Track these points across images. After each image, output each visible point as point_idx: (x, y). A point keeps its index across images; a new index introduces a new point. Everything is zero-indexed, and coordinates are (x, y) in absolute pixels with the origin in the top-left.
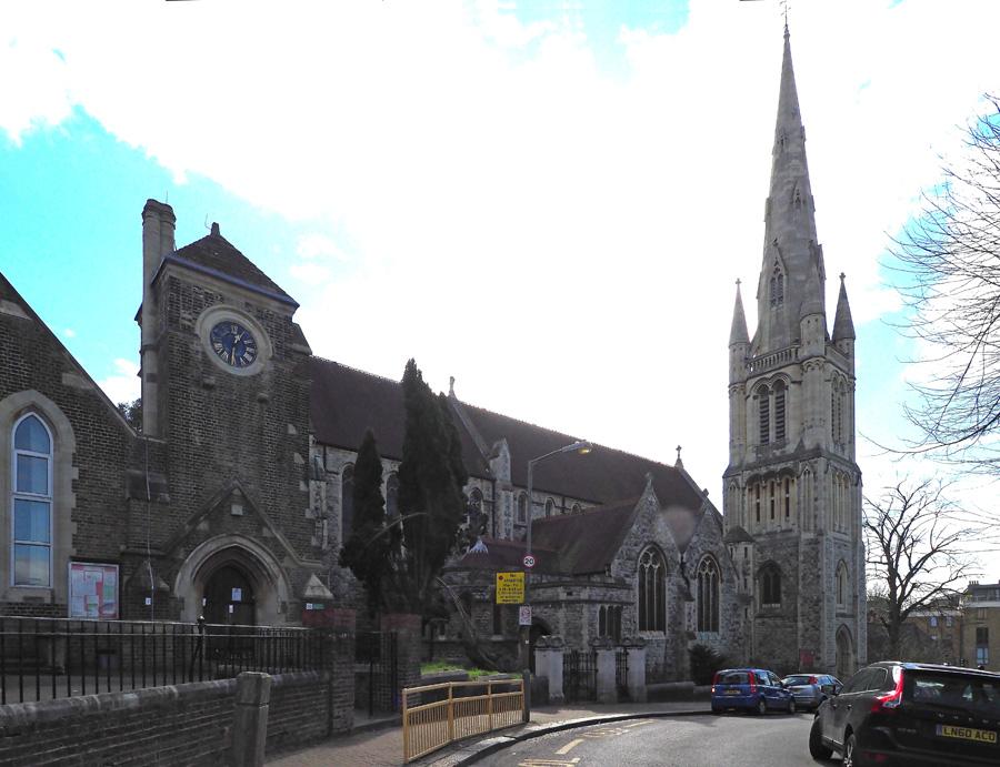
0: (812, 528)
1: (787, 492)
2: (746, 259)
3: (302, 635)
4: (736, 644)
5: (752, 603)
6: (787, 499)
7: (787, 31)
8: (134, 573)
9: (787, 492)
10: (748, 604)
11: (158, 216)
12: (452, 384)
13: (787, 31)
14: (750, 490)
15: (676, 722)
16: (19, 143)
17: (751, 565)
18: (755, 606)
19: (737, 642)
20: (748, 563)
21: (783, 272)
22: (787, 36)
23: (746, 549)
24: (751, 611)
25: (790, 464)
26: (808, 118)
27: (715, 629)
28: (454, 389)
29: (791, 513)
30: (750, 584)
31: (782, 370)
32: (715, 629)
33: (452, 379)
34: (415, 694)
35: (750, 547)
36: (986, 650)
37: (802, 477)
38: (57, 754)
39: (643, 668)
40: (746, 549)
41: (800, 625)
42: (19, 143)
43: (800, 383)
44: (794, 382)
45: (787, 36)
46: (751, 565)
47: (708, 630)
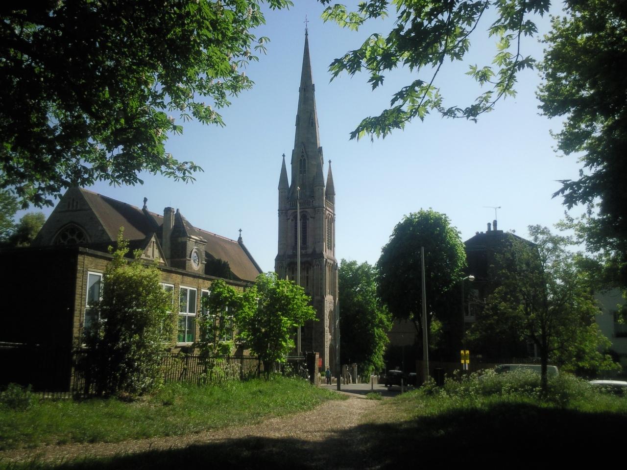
0: (319, 294)
1: (308, 273)
2: (286, 142)
6: (307, 277)
7: (306, 32)
9: (308, 273)
12: (145, 203)
13: (306, 32)
14: (289, 269)
21: (305, 156)
22: (307, 34)
25: (309, 259)
26: (315, 80)
28: (147, 205)
29: (309, 285)
31: (307, 210)
33: (145, 200)
34: (421, 268)
36: (81, 249)
37: (315, 267)
38: (8, 345)
41: (314, 344)
43: (314, 218)
44: (311, 217)
45: (307, 34)
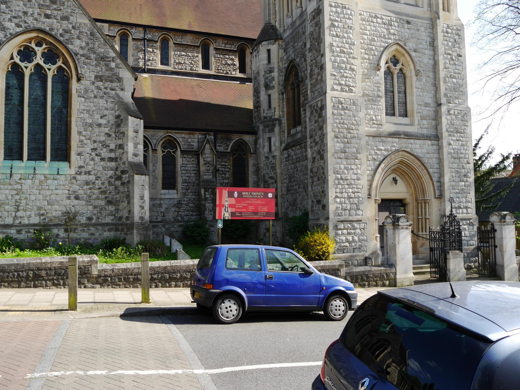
3: (380, 283)
4: (118, 183)
5: (277, 129)
8: (172, 273)
10: (272, 130)
11: (192, 302)
15: (162, 307)
16: (195, 305)
17: (275, 74)
18: (281, 132)
19: (119, 178)
20: (271, 71)
23: (269, 51)
24: (275, 141)
27: (62, 154)
30: (275, 103)
32: (62, 154)
35: (274, 48)
39: (429, 142)
40: (269, 51)
42: (195, 305)
46: (275, 74)
47: (38, 154)
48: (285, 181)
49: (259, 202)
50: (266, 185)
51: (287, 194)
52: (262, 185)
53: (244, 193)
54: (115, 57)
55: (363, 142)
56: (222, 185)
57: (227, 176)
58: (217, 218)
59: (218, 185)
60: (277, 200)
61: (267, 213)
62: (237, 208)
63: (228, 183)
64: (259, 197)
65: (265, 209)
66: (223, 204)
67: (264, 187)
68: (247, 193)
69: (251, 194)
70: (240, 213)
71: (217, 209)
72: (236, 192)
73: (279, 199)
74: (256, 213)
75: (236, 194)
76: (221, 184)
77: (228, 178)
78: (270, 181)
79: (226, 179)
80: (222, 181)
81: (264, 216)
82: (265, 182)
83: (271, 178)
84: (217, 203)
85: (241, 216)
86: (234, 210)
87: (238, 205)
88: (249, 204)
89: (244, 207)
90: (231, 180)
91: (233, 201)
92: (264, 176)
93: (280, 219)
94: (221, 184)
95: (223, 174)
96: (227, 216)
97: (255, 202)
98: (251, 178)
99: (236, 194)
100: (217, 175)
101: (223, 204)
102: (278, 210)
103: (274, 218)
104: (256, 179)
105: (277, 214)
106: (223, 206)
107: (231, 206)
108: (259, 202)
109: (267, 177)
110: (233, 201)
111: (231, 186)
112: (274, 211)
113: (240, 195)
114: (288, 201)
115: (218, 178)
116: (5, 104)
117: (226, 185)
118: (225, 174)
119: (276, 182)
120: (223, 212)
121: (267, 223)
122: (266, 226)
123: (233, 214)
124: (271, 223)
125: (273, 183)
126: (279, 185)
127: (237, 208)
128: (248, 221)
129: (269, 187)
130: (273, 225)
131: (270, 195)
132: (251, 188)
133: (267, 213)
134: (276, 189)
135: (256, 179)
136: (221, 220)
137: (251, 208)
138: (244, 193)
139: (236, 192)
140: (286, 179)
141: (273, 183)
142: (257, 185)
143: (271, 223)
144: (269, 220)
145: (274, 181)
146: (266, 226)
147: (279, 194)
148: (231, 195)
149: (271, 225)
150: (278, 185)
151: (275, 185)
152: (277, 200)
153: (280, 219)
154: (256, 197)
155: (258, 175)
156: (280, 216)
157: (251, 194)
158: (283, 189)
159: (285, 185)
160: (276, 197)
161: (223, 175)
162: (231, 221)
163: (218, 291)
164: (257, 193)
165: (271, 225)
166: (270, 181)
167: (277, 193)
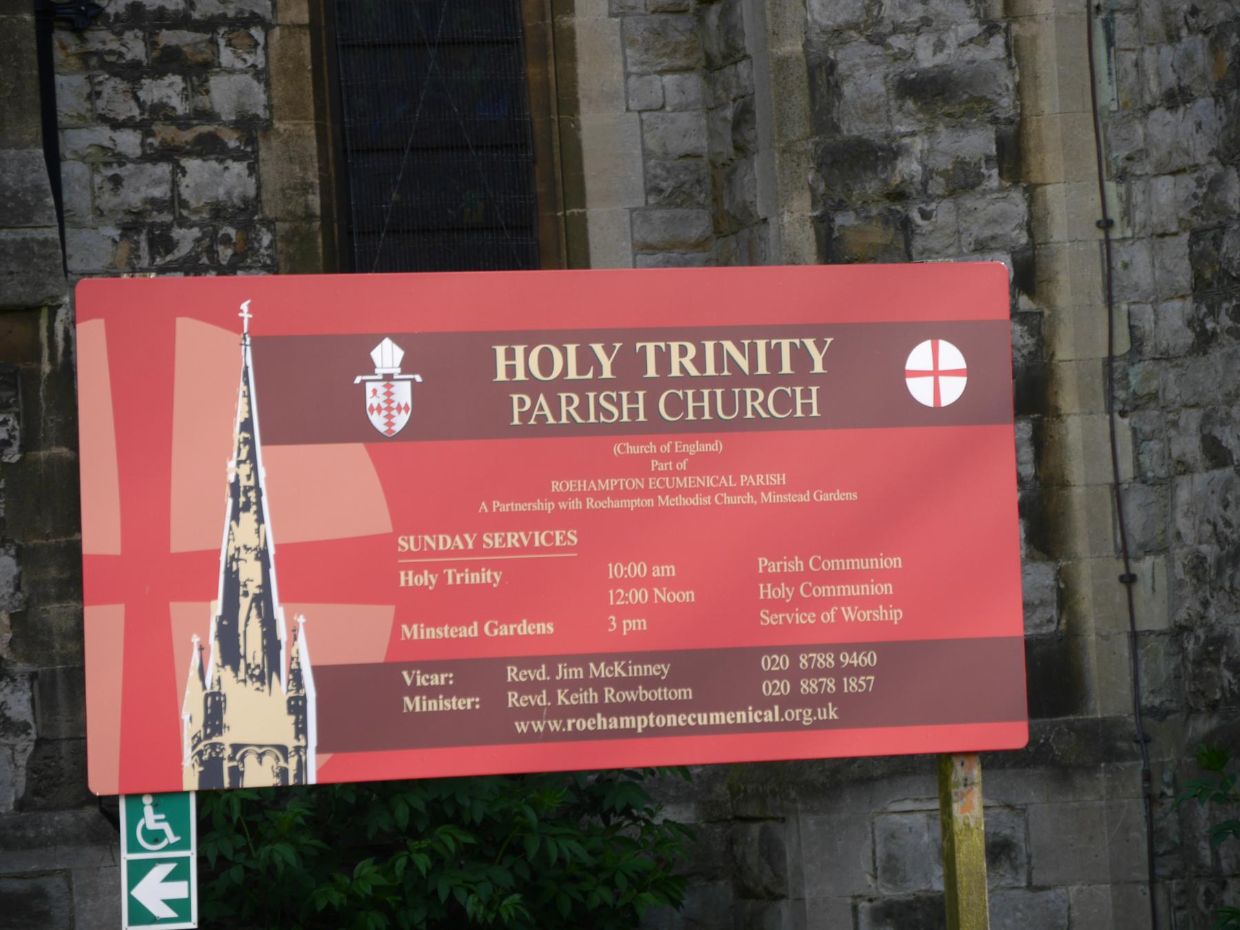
48: (1165, 128)
49: (767, 487)
50: (866, 210)
51: (1204, 341)
52: (795, 219)
53: (514, 362)
54: (311, 185)
55: (301, 200)
56: (148, 236)
57: (228, 92)
58: (103, 777)
59: (94, 243)
60: (1043, 444)
61: (897, 656)
62: (414, 606)
63: (245, 214)
64: (757, 403)
65: (867, 598)
66: (182, 540)
67: (831, 250)
68: (566, 361)
69: (629, 367)
70: (476, 671)
71: (104, 629)
72: (388, 355)
73: (1081, 427)
74: (716, 671)
75: (389, 385)
76: (132, 225)
77: (247, 125)
78: (924, 148)
79: (209, 147)
80: (148, 184)
81: (854, 711)
82: (848, 160)
83: (929, 92)
84: (101, 531)
85: (493, 723)
86: (364, 634)
87: (440, 554)
88: (607, 535)
89: (526, 585)
90: (293, 164)
91: (338, 491)
92: (823, 77)
93: (1103, 745)
94: (132, 225)
95: (168, 61)
96: (266, 733)
97: (695, 493)
98: (621, 107)
99: (389, 385)
100: (70, 89)
101: (182, 540)
102: (1065, 597)
103: (1014, 734)
104: (687, 131)
105: (1052, 674)
106: (199, 573)
107: (313, 571)
108: (767, 487)
109: (865, 79)
110: (338, 491)
111: (295, 259)
112: (1002, 615)
113: (456, 392)
114: (1216, 454)
115: (76, 140)
116: (569, 268)
117: (229, 245)
118: (198, 72)
119: (1013, 156)
120: (198, 673)
121: (906, 813)
122: (890, 869)
123: (351, 699)
124: (971, 811)
125: (963, 180)
126: (1070, 200)
127: (414, 606)
128: (597, 797)
129: (902, 244)
130: (998, 850)
131: (937, 373)
132: (615, 275)
133: (903, 664)
134: (1028, 275)
135: (687, 131)
136: (168, 799)
137: (643, 594)
138: (514, 362)
139: (388, 355)
140: (1176, 98)
141: (963, 180)
142: (713, 218)
143: (971, 811)
144: (936, 767)
145: (979, 142)
146: (890, 869)
147: (1077, 349)
148: (306, 400)
149: (971, 849)
150: (1056, 196)
151: (999, 208)
152: (1043, 444)
153: (1103, 745)
154: (710, 404)
155: (716, 62)
156: (1109, 692)
157: (629, 367)
158: (1140, 265)
159: (1166, 197)
160: (1033, 393)
161: (167, 90)
162: (338, 818)
163: (320, 240)
164: (732, 340)
165: (971, 849)
166: (924, 148)
167: (1037, 326)
